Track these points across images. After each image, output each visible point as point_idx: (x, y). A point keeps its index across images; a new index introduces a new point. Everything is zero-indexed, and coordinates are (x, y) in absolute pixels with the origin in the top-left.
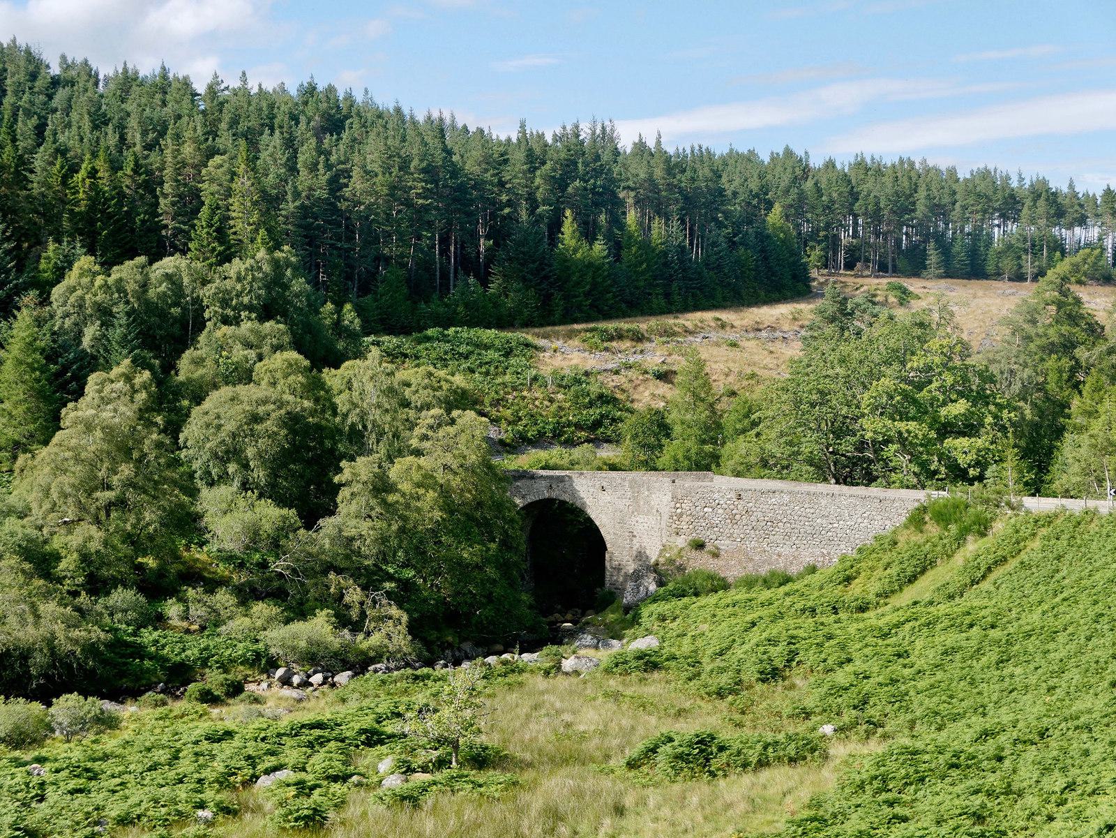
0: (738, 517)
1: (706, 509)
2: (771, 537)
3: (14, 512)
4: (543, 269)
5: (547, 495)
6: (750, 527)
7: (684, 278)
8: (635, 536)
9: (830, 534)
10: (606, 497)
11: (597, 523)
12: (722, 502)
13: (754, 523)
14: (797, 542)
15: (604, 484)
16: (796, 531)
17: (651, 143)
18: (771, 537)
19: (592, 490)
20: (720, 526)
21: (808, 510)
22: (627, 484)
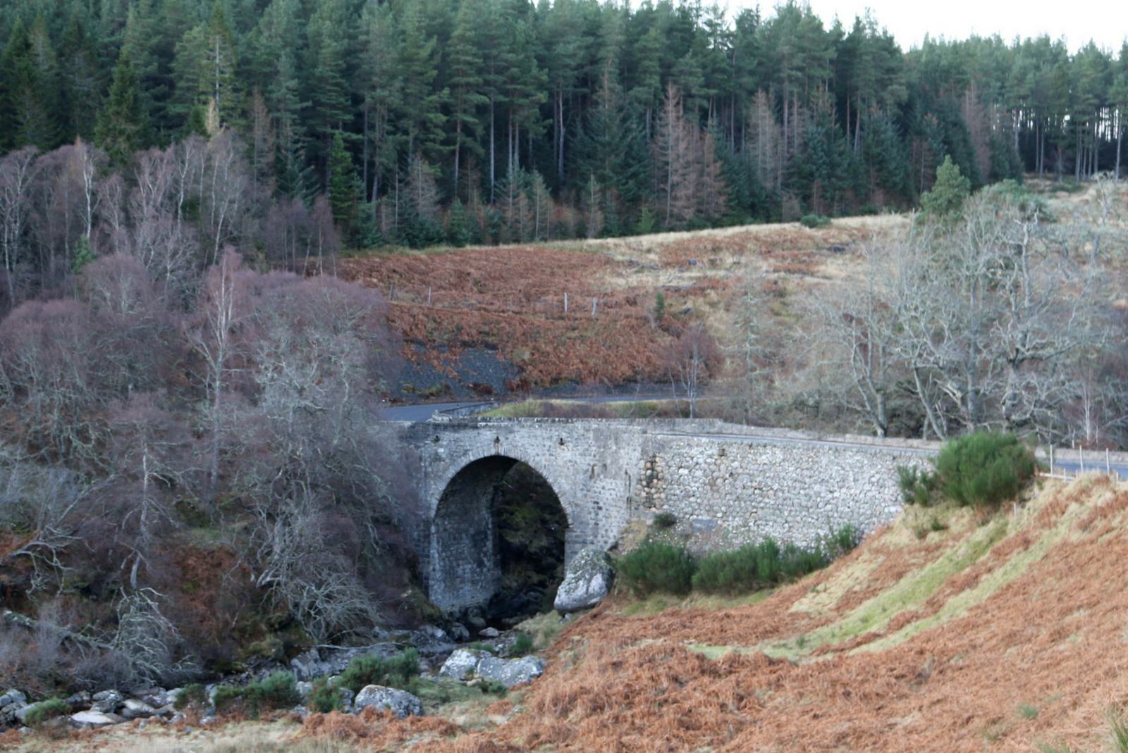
0: (719, 481)
1: (681, 471)
2: (760, 512)
3: (452, 567)
4: (630, 166)
5: (493, 452)
6: (734, 497)
7: (829, 177)
8: (600, 508)
9: (829, 507)
10: (566, 454)
11: (556, 489)
12: (701, 461)
13: (739, 491)
14: (789, 519)
15: (564, 435)
16: (789, 502)
17: (1053, 41)
18: (760, 512)
19: (548, 443)
20: (698, 494)
21: (806, 472)
22: (591, 435)
